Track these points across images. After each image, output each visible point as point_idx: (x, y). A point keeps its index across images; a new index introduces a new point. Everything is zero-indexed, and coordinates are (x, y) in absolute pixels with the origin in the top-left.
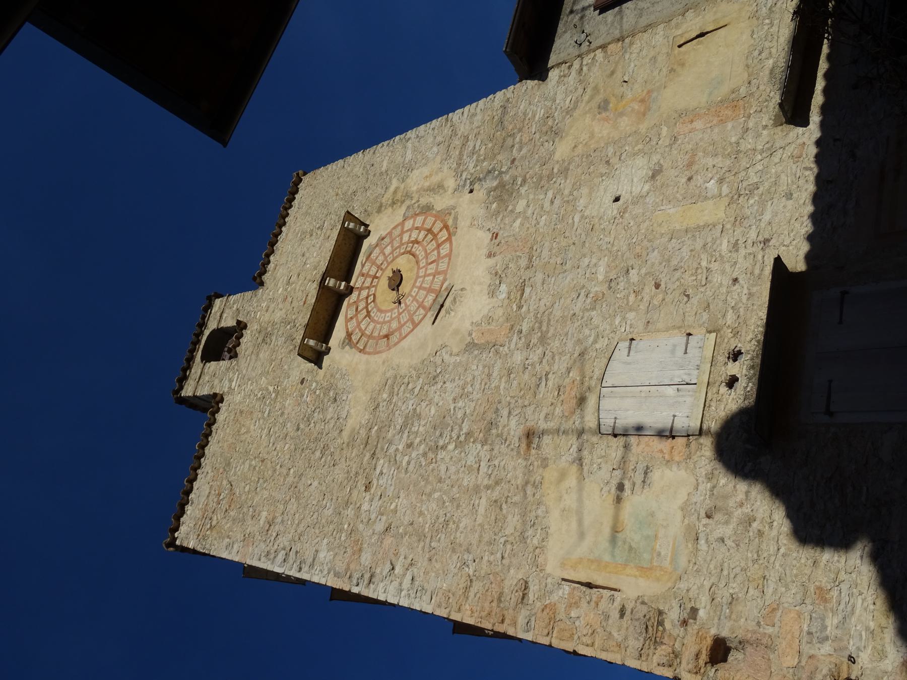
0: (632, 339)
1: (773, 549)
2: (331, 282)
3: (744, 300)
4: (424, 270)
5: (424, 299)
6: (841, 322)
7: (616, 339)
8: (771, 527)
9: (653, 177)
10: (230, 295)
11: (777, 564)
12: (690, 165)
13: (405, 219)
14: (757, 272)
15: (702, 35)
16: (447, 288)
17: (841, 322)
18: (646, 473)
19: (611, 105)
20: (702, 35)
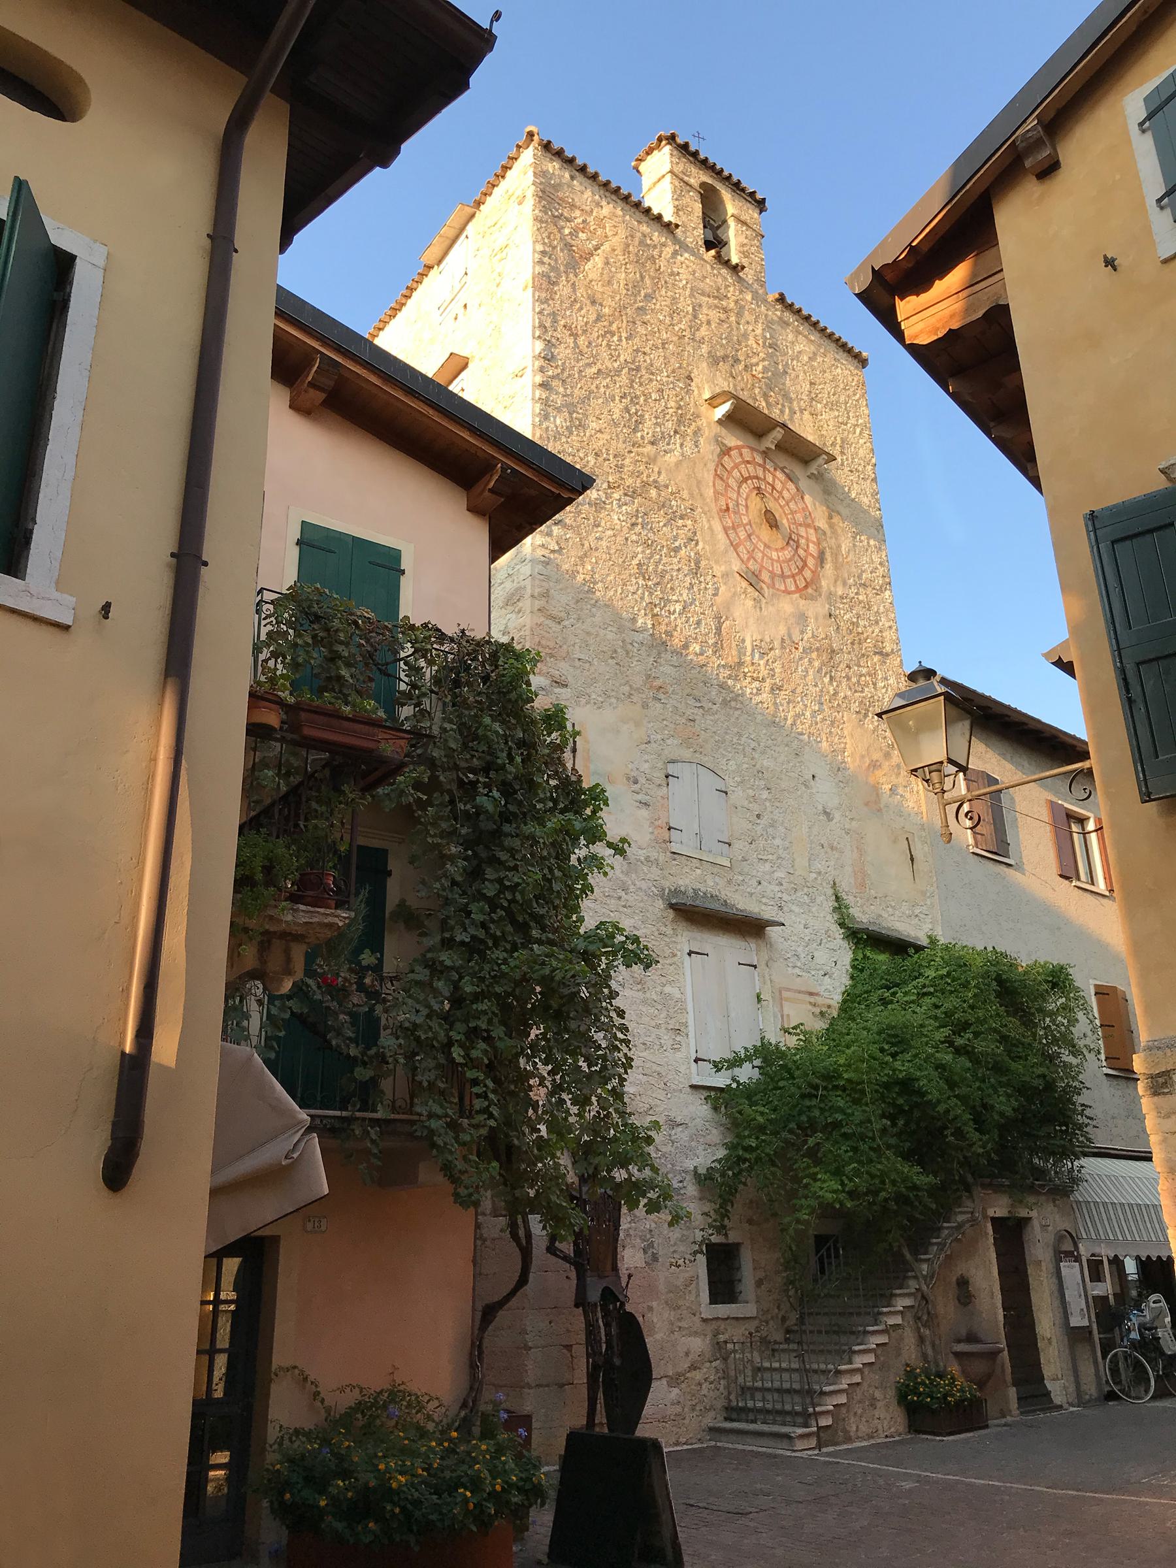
0: (726, 793)
1: (612, 907)
2: (778, 434)
3: (748, 890)
4: (762, 549)
5: (795, 582)
6: (739, 964)
7: (726, 778)
8: (624, 906)
9: (825, 813)
10: (701, 194)
11: (604, 910)
12: (832, 848)
13: (816, 529)
14: (764, 900)
15: (912, 859)
16: (762, 588)
17: (739, 964)
18: (645, 804)
19: (400, 778)
20: (912, 859)
